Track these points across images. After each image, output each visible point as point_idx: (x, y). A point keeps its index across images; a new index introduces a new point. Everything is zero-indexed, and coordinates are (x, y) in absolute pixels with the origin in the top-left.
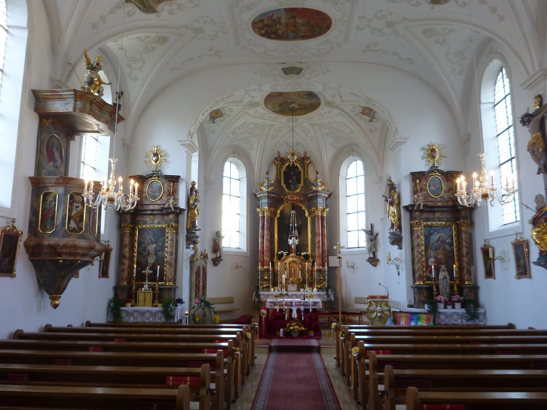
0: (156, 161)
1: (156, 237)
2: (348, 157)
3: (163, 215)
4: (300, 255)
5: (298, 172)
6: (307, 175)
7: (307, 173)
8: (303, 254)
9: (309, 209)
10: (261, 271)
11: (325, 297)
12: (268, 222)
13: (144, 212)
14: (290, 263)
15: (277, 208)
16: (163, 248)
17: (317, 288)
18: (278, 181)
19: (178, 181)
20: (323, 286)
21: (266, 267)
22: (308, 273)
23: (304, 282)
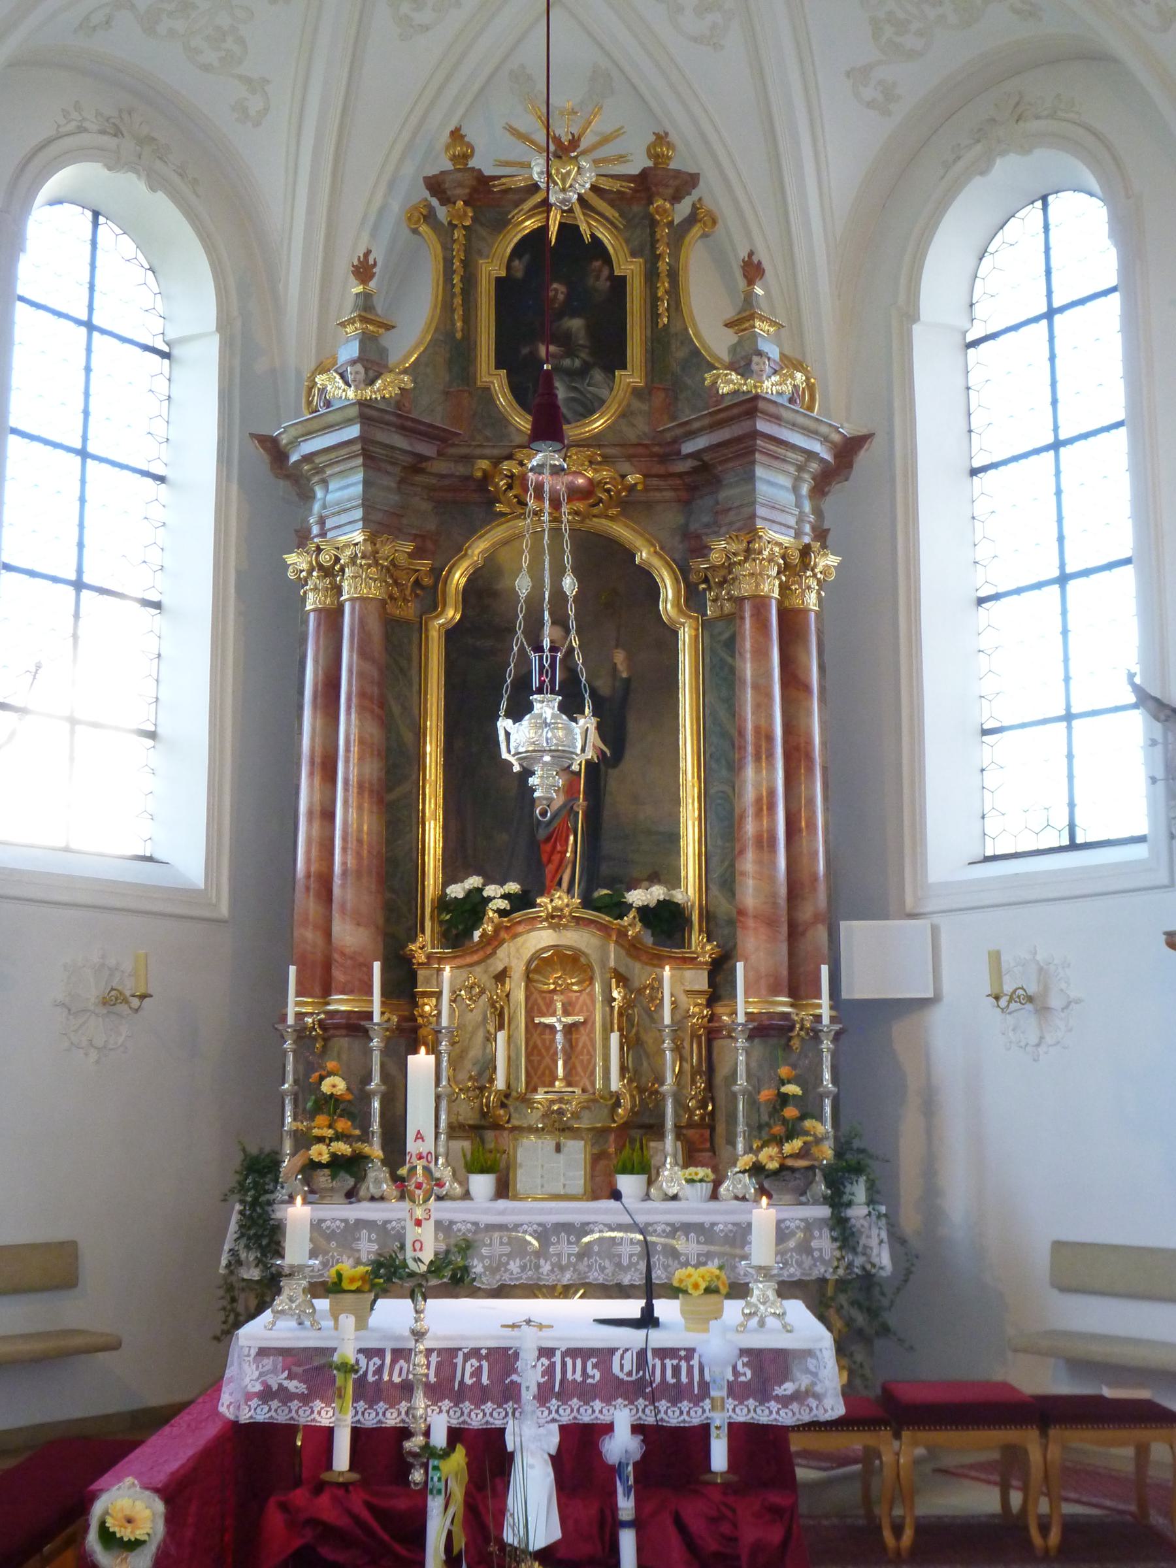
2: (983, 167)
4: (619, 908)
5: (603, 284)
6: (676, 305)
7: (675, 292)
8: (637, 897)
9: (688, 550)
10: (302, 1035)
11: (824, 1244)
12: (363, 651)
14: (538, 966)
15: (439, 547)
17: (757, 1170)
18: (452, 350)
20: (804, 1153)
21: (341, 1003)
22: (677, 1049)
23: (646, 1124)
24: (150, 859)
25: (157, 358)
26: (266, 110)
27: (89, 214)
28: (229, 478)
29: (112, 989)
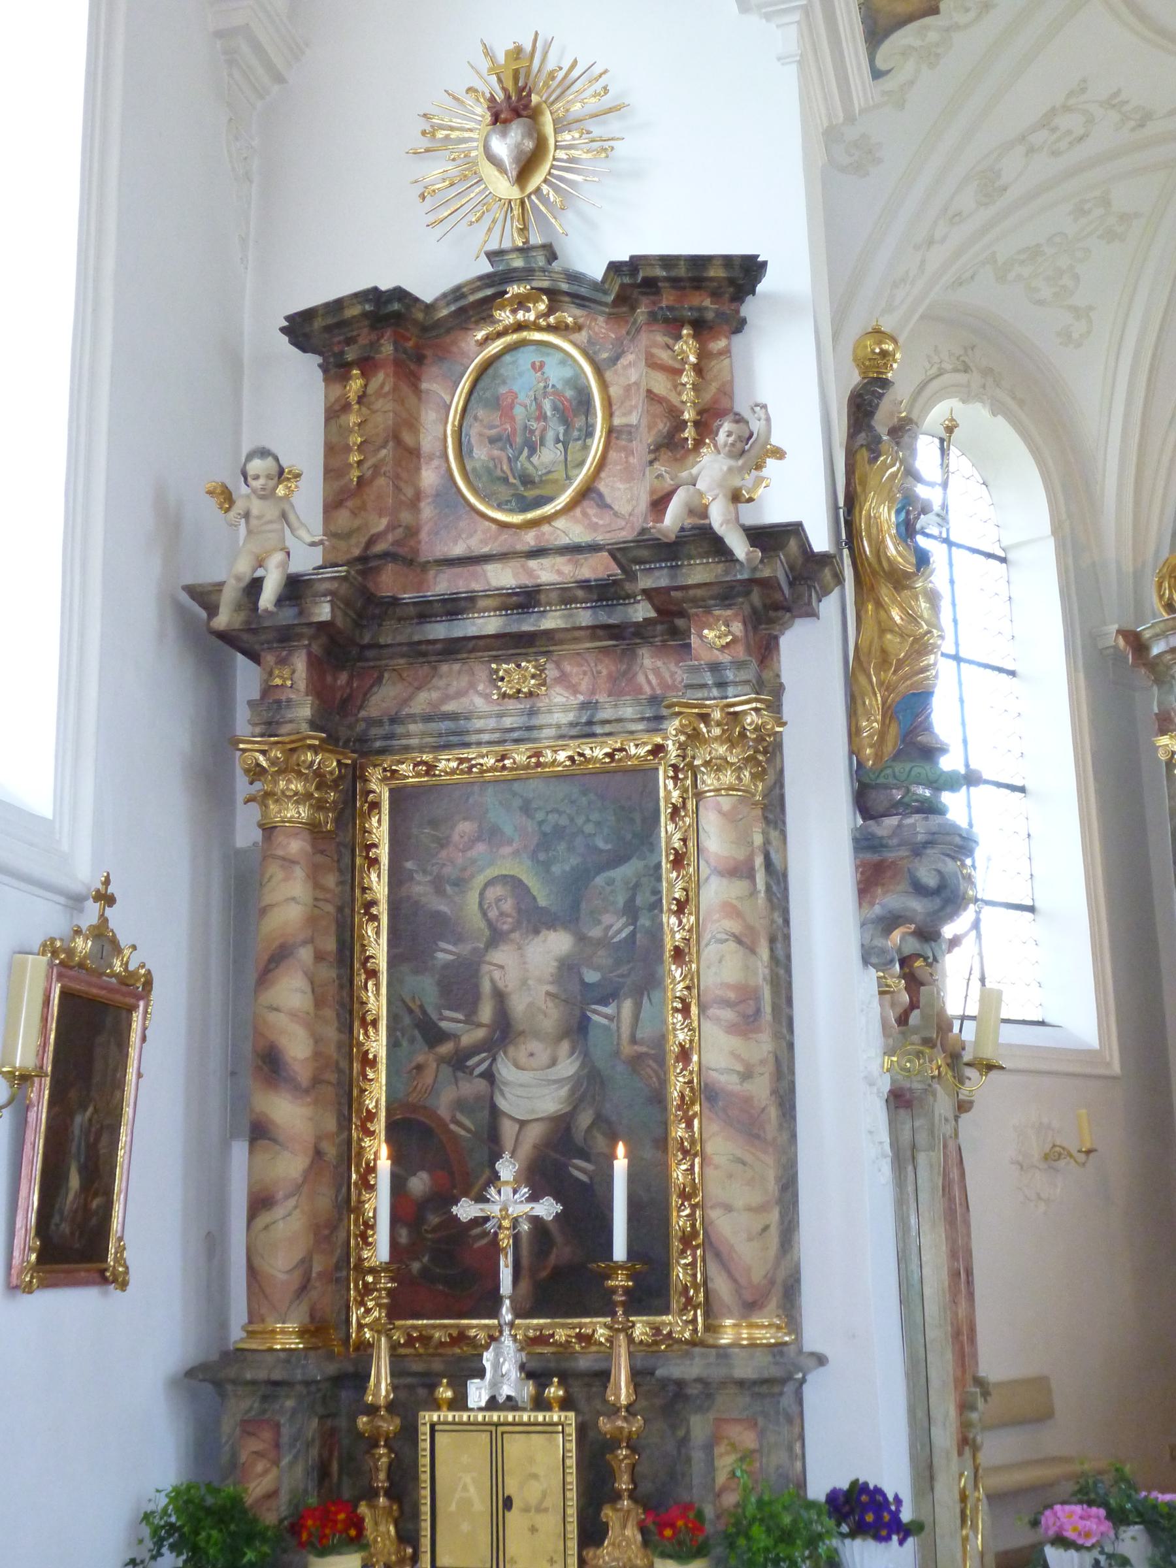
0: (526, 166)
1: (566, 863)
3: (621, 639)
13: (439, 631)
16: (639, 964)
19: (739, 326)
24: (1042, 1023)
25: (997, 563)
26: (1089, 332)
27: (937, 441)
28: (1076, 670)
29: (1054, 1146)
